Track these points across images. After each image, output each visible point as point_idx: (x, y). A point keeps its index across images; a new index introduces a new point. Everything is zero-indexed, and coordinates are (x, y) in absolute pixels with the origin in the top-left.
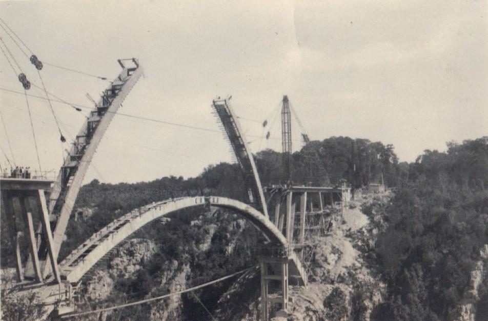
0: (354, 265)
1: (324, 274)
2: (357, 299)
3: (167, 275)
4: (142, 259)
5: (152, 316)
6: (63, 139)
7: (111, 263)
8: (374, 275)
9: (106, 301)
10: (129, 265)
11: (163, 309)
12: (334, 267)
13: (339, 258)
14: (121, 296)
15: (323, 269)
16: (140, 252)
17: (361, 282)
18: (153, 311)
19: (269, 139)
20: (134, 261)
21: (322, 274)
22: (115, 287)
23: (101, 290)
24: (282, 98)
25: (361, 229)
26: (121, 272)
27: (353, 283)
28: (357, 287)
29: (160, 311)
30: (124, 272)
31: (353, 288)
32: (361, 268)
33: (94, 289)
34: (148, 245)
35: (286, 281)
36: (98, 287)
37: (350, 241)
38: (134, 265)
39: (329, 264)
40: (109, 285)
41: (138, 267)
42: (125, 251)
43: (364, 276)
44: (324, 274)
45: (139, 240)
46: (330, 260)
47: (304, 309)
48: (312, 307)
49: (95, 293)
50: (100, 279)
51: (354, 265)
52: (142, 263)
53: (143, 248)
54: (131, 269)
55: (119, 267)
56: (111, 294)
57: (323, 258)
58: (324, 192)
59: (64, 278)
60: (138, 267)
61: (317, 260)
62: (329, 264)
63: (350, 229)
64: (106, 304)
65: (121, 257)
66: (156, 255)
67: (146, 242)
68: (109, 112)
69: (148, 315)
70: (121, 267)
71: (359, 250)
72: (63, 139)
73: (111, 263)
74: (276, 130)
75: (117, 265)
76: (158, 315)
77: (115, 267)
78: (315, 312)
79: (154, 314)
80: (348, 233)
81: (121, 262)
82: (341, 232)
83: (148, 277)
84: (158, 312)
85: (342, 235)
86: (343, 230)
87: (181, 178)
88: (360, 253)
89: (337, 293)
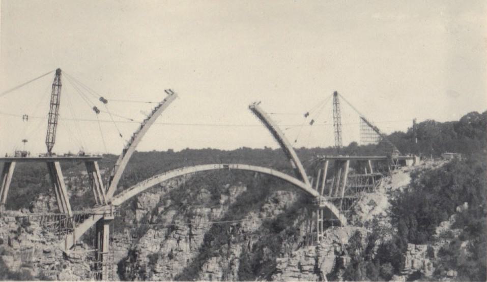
0: (381, 214)
1: (357, 219)
2: (371, 238)
3: (300, 218)
4: (285, 206)
5: (283, 246)
6: (272, 114)
7: (262, 207)
8: (392, 222)
9: (254, 233)
10: (275, 209)
11: (292, 242)
12: (366, 214)
13: (373, 209)
14: (265, 231)
15: (357, 216)
16: (284, 201)
17: (380, 227)
18: (284, 243)
19: (313, 126)
20: (279, 207)
21: (356, 220)
22: (263, 225)
23: (251, 226)
24: (333, 93)
25: (399, 188)
26: (270, 214)
27: (373, 227)
28: (377, 230)
29: (290, 243)
30: (271, 214)
31: (373, 230)
32: (385, 217)
33: (246, 225)
34: (290, 196)
35: (320, 224)
36: (249, 223)
37: (388, 197)
38: (279, 209)
39: (363, 212)
40: (257, 223)
41: (281, 211)
42: (272, 200)
43: (385, 223)
44: (357, 219)
45: (283, 191)
46: (363, 210)
47: (332, 242)
48: (337, 240)
49: (247, 228)
50: (251, 218)
51: (381, 214)
52: (284, 209)
53: (286, 198)
54: (277, 212)
55: (269, 211)
56: (259, 228)
57: (358, 208)
58: (374, 159)
59: (109, 203)
60: (281, 211)
61: (225, 201)
62: (363, 212)
63: (391, 188)
64: (253, 235)
65: (269, 204)
66: (295, 204)
67: (289, 193)
68: (146, 115)
69: (280, 245)
70: (270, 211)
71: (391, 203)
72: (272, 114)
73: (262, 207)
74: (325, 116)
75: (267, 209)
76: (288, 245)
77: (265, 210)
78: (340, 245)
79: (285, 245)
80: (389, 191)
81: (269, 207)
82: (384, 190)
83: (285, 219)
84: (289, 243)
85: (384, 192)
86: (385, 189)
87: (240, 148)
88: (391, 205)
89: (357, 234)
